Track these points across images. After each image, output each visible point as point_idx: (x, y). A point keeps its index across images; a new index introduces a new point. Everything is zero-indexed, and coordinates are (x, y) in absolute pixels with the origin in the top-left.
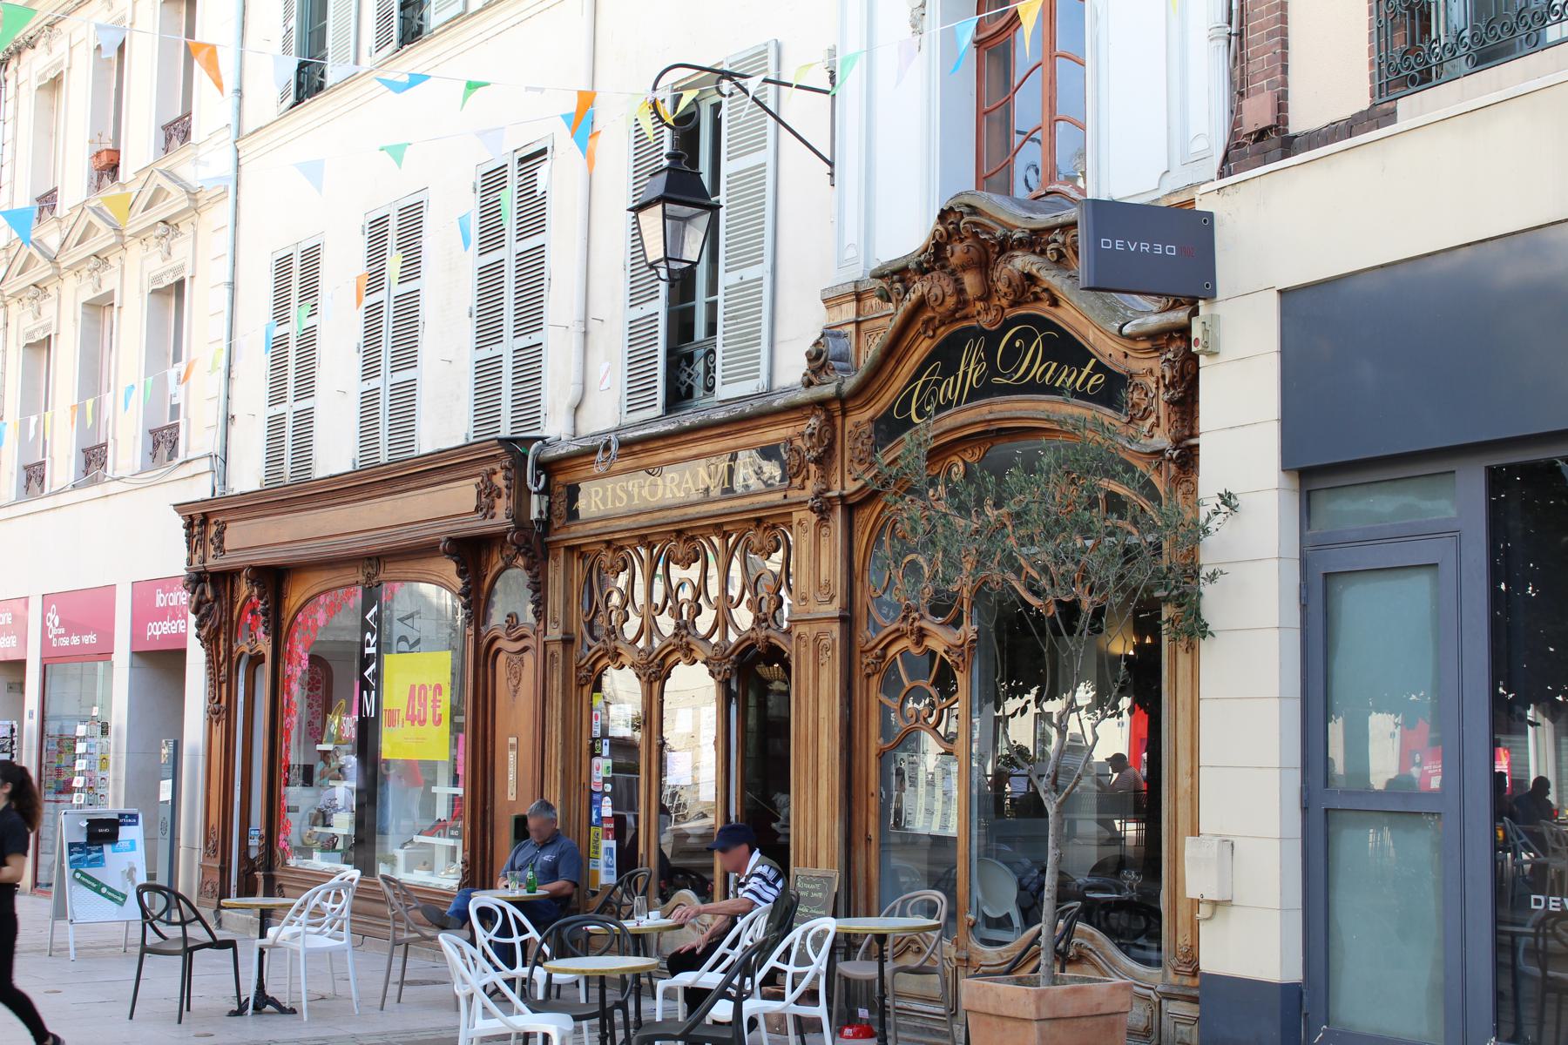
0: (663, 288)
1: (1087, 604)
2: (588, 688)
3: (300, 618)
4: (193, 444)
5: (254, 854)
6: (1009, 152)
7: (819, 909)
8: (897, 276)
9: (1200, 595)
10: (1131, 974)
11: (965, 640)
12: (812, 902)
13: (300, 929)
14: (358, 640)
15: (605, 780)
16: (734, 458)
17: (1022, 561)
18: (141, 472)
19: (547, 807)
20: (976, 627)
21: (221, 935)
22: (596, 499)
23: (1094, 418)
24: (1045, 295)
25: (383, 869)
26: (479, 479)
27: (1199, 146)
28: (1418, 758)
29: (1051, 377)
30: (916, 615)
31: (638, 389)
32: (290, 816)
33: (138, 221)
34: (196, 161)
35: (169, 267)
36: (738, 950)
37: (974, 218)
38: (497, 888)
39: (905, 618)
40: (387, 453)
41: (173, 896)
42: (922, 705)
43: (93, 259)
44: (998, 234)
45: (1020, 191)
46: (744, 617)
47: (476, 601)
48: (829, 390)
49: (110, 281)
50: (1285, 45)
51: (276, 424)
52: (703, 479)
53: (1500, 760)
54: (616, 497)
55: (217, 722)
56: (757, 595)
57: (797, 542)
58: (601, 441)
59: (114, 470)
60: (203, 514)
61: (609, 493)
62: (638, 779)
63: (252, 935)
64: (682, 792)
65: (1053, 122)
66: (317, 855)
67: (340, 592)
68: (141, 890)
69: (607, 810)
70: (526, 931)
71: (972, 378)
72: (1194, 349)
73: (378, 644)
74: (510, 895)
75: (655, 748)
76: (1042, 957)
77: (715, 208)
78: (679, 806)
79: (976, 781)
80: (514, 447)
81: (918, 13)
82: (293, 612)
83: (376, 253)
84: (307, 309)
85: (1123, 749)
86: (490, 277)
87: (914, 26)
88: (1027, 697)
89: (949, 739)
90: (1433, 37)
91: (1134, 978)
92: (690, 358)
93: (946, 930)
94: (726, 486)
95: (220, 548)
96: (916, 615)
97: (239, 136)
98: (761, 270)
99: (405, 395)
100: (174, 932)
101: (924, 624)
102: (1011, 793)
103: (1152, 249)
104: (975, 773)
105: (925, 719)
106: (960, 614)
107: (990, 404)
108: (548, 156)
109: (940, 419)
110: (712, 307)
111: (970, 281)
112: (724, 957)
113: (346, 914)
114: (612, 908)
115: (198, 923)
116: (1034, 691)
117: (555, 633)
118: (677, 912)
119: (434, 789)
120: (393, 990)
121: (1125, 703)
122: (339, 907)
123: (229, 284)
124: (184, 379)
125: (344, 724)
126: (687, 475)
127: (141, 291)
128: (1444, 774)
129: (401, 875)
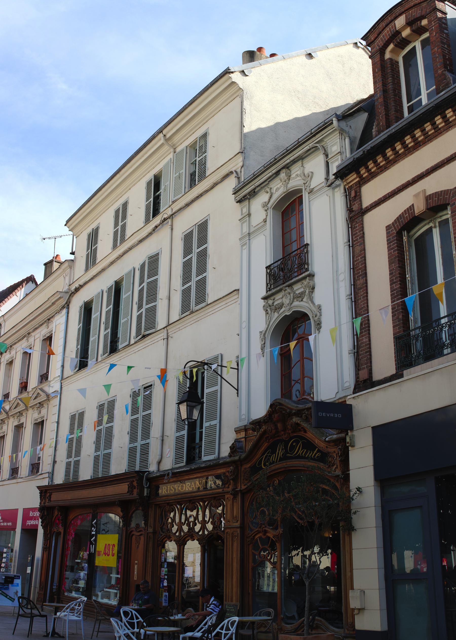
0: (186, 427)
1: (317, 522)
2: (160, 547)
3: (72, 522)
4: (44, 469)
5: (54, 591)
6: (291, 387)
7: (233, 614)
8: (256, 424)
9: (351, 518)
10: (333, 631)
11: (279, 533)
12: (230, 612)
13: (67, 614)
14: (90, 529)
15: (165, 575)
16: (207, 478)
17: (296, 509)
18: (28, 476)
19: (146, 582)
20: (282, 530)
21: (42, 613)
22: (164, 490)
23: (318, 466)
24: (302, 429)
25: (94, 598)
26: (129, 483)
27: (347, 385)
28: (419, 563)
29: (304, 454)
30: (264, 526)
31: (178, 458)
32: (66, 580)
33: (32, 403)
34: (49, 386)
35: (40, 416)
36: (206, 626)
37: (281, 407)
38: (130, 605)
39: (260, 527)
40: (101, 474)
41: (29, 601)
42: (266, 553)
43: (18, 413)
44: (288, 411)
45: (294, 398)
46: (210, 527)
47: (126, 519)
48: (237, 458)
49: (23, 420)
50: (370, 355)
51: (68, 464)
52: (198, 485)
53: (444, 561)
54: (170, 489)
55: (46, 551)
56: (214, 520)
57: (226, 504)
58: (167, 472)
59: (20, 475)
60: (45, 490)
61: (169, 489)
62: (176, 575)
63: (52, 614)
64: (190, 579)
65: (304, 378)
66: (74, 592)
67: (85, 515)
68: (19, 598)
69: (165, 584)
70: (139, 619)
71: (281, 454)
72: (347, 445)
73: (96, 531)
74: (134, 608)
75: (181, 565)
76: (305, 627)
77: (203, 403)
78: (188, 583)
79: (283, 576)
80: (140, 475)
81: (263, 346)
82: (71, 520)
83: (100, 414)
84: (79, 431)
85: (329, 565)
86: (134, 423)
87: (262, 350)
88: (299, 550)
89: (274, 564)
90: (413, 353)
91: (334, 632)
92: (194, 448)
93: (274, 620)
94: (205, 487)
95: (50, 500)
96: (264, 526)
97: (62, 379)
98: (216, 422)
99: (107, 457)
100: (29, 611)
101: (266, 529)
102: (294, 579)
103: (334, 415)
104: (283, 574)
105: (267, 558)
106: (278, 525)
107: (286, 462)
108: (153, 387)
109: (271, 467)
110: (201, 433)
111: (279, 425)
112: (202, 628)
113: (81, 610)
114: (167, 612)
115: (36, 609)
116: (301, 548)
117: (150, 530)
118: (187, 615)
119: (111, 575)
120: (95, 633)
121: (329, 551)
122: (80, 608)
123: (57, 422)
124: (42, 449)
125: (84, 554)
126: (193, 483)
127: (32, 423)
128: (428, 567)
129: (100, 600)
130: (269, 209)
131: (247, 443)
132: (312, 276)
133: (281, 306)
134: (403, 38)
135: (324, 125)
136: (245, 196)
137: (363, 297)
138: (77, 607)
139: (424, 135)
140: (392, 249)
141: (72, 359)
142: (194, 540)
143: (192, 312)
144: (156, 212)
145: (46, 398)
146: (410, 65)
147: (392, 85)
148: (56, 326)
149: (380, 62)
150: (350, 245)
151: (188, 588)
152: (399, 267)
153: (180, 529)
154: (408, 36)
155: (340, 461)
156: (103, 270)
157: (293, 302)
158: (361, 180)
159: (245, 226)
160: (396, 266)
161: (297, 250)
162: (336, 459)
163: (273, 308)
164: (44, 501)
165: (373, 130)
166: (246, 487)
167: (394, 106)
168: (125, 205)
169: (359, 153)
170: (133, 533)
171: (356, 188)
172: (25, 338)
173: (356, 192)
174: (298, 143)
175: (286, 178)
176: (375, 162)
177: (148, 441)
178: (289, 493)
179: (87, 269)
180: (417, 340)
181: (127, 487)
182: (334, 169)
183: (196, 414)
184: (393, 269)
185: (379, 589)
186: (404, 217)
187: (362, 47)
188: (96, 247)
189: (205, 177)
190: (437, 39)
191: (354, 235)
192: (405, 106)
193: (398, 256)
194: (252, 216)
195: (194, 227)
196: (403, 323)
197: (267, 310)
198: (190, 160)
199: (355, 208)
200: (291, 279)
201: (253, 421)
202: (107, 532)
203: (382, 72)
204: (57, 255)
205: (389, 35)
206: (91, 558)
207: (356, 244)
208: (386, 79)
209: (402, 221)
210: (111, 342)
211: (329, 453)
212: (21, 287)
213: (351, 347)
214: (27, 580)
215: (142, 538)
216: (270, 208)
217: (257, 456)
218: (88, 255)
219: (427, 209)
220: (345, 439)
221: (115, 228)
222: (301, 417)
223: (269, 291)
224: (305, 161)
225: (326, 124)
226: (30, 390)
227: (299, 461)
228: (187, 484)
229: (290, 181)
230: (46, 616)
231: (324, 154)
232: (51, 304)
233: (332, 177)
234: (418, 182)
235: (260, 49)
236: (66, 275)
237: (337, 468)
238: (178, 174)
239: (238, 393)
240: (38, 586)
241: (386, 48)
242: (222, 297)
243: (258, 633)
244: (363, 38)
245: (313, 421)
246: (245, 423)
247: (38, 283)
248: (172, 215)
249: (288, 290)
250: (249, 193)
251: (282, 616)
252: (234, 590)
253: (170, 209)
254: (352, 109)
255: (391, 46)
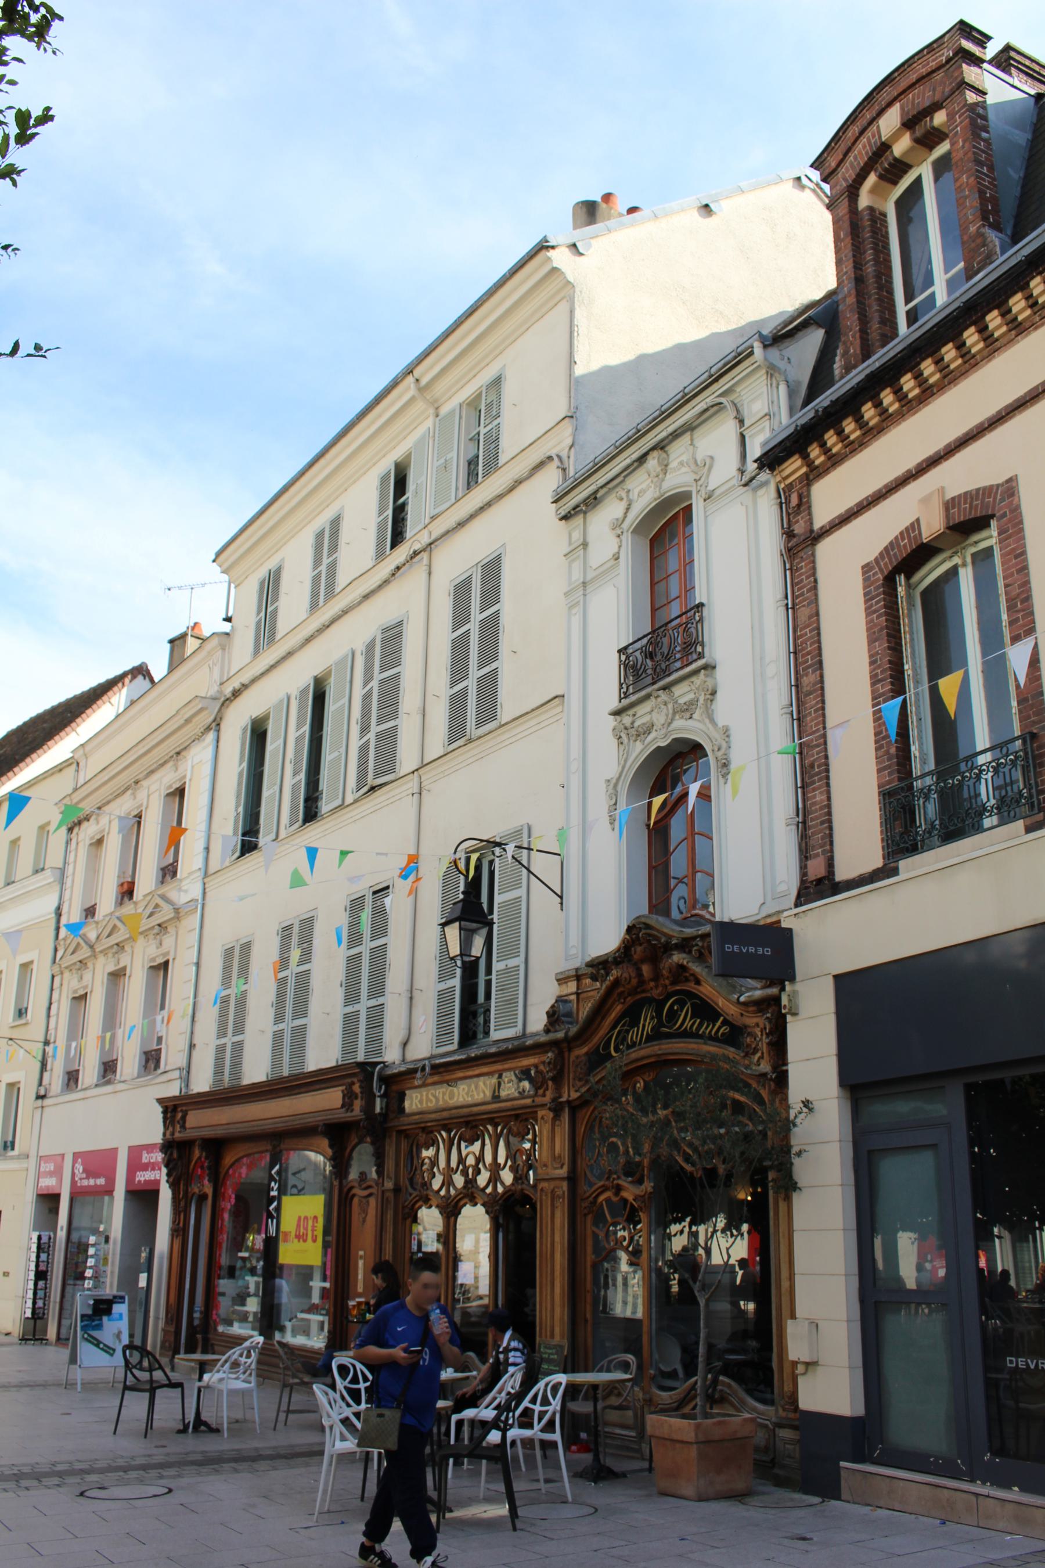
0: (458, 972)
1: (722, 1169)
2: (408, 1221)
3: (231, 1172)
4: (170, 1060)
5: (196, 1322)
6: (668, 891)
8: (600, 966)
9: (792, 1164)
12: (550, 1361)
13: (224, 1375)
16: (500, 1076)
21: (175, 1377)
22: (416, 1101)
24: (692, 978)
27: (782, 888)
31: (443, 1033)
33: (145, 924)
34: (180, 890)
36: (503, 1394)
39: (608, 1179)
45: (675, 914)
46: (507, 1177)
47: (340, 1163)
48: (560, 1035)
51: (220, 1050)
57: (540, 1131)
58: (420, 1065)
61: (424, 1098)
65: (694, 872)
66: (236, 1325)
67: (256, 1156)
71: (648, 1028)
72: (783, 1011)
73: (279, 1189)
75: (451, 1260)
77: (490, 924)
80: (365, 1069)
84: (242, 981)
85: (744, 1254)
86: (353, 963)
88: (683, 1224)
92: (475, 1015)
95: (183, 1127)
97: (206, 875)
99: (300, 1035)
101: (620, 1182)
103: (756, 950)
106: (642, 1176)
108: (390, 890)
110: (488, 983)
111: (646, 969)
113: (253, 1366)
116: (688, 1219)
117: (389, 1185)
120: (282, 1416)
121: (745, 1227)
125: (255, 1240)
127: (143, 967)
128: (947, 1267)
130: (625, 534)
131: (581, 1004)
132: (710, 667)
133: (649, 729)
134: (895, 159)
135: (736, 357)
136: (577, 506)
137: (816, 711)
138: (243, 1360)
139: (941, 371)
140: (875, 612)
141: (224, 837)
142: (475, 1205)
143: (470, 741)
144: (398, 537)
145: (172, 915)
146: (910, 220)
147: (874, 265)
148: (193, 767)
149: (847, 217)
150: (787, 605)
151: (464, 1302)
152: (889, 648)
153: (448, 1182)
154: (909, 151)
155: (769, 1044)
156: (290, 654)
157: (672, 720)
158: (811, 471)
159: (577, 566)
160: (881, 646)
161: (680, 616)
162: (761, 1040)
163: (633, 732)
164: (171, 1129)
165: (836, 366)
166: (578, 1094)
167: (878, 311)
168: (336, 524)
169: (806, 415)
170: (354, 1191)
171: (801, 488)
172: (129, 792)
173: (800, 497)
174: (683, 397)
175: (659, 469)
176: (840, 432)
177: (381, 1000)
178: (665, 1107)
179: (257, 652)
180: (927, 798)
181: (340, 1095)
182: (755, 450)
183: (477, 948)
184: (877, 653)
185: (848, 1321)
186: (898, 545)
187: (811, 185)
188: (276, 609)
189: (497, 468)
190: (965, 154)
191: (797, 584)
192: (901, 309)
193: (887, 627)
194: (590, 548)
195: (474, 569)
196: (898, 764)
197: (620, 737)
198: (467, 432)
199: (799, 528)
200: (669, 675)
201: (593, 960)
202: (300, 1192)
203: (852, 239)
204: (196, 624)
205: (867, 153)
206: (271, 1246)
207: (800, 602)
208: (861, 254)
209: (895, 554)
210: (306, 800)
211: (746, 1027)
212: (120, 685)
213: (792, 812)
214: (141, 1303)
215: (372, 1201)
217: (602, 1032)
218: (258, 623)
219: (949, 528)
220: (777, 1000)
221: (315, 569)
222: (690, 952)
223: (625, 698)
224: (697, 433)
225: (740, 354)
226: (140, 897)
228: (462, 1087)
229: (668, 476)
230: (180, 1385)
231: (736, 418)
232: (182, 721)
233: (751, 467)
234: (928, 471)
235: (607, 197)
236: (214, 664)
237: (762, 1057)
238: (442, 461)
239: (562, 904)
240: (162, 1314)
241: (861, 184)
242: (529, 709)
243: (605, 1408)
244: (817, 164)
245: (713, 960)
246: (577, 963)
247: (156, 680)
248: (431, 544)
249: (663, 696)
250: (585, 501)
251: (652, 1372)
253: (426, 531)
254: (791, 322)
255: (872, 179)
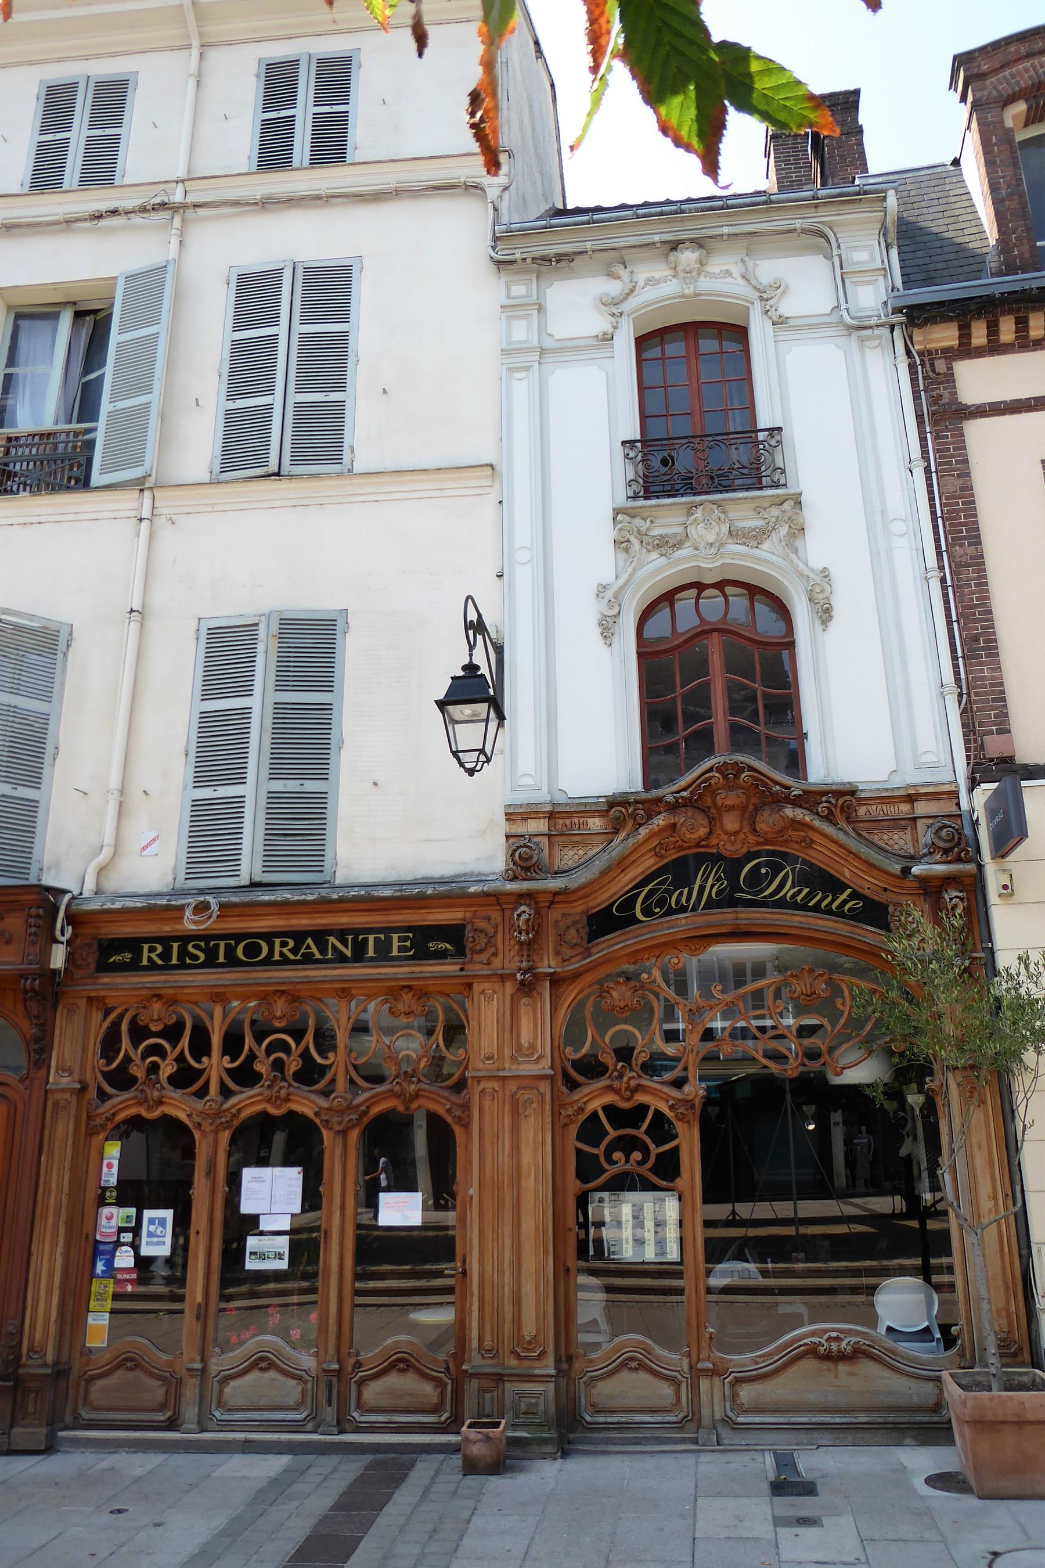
216: (628, 315)
227: (804, 916)
252: (530, 1261)
